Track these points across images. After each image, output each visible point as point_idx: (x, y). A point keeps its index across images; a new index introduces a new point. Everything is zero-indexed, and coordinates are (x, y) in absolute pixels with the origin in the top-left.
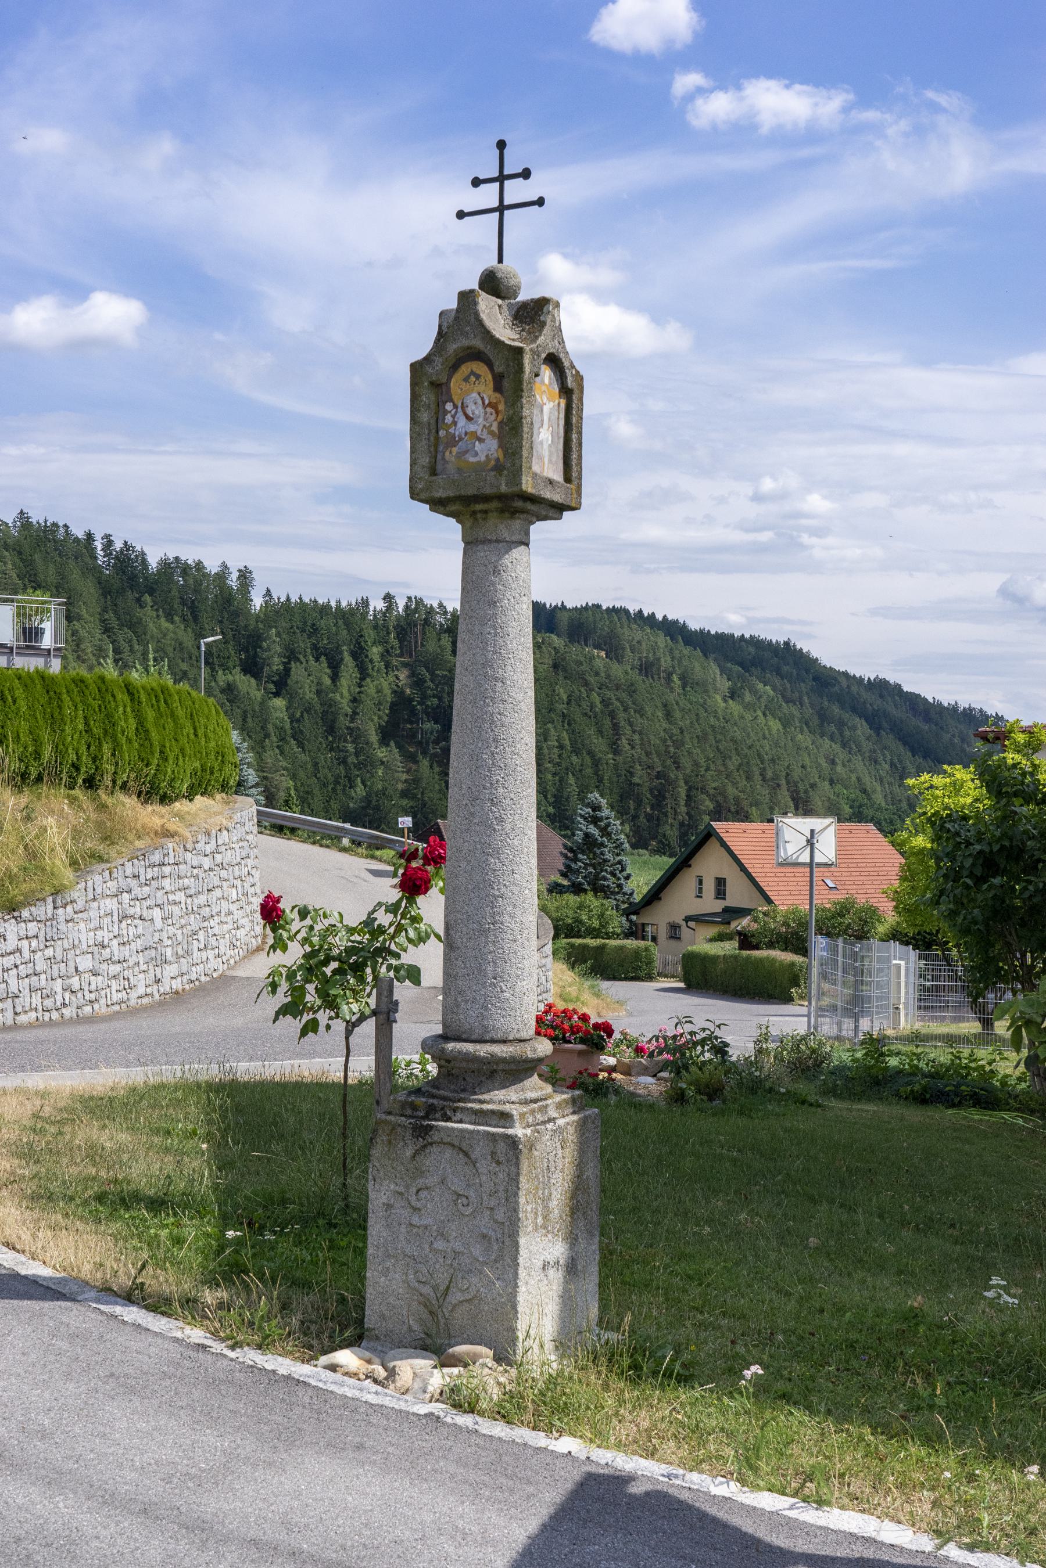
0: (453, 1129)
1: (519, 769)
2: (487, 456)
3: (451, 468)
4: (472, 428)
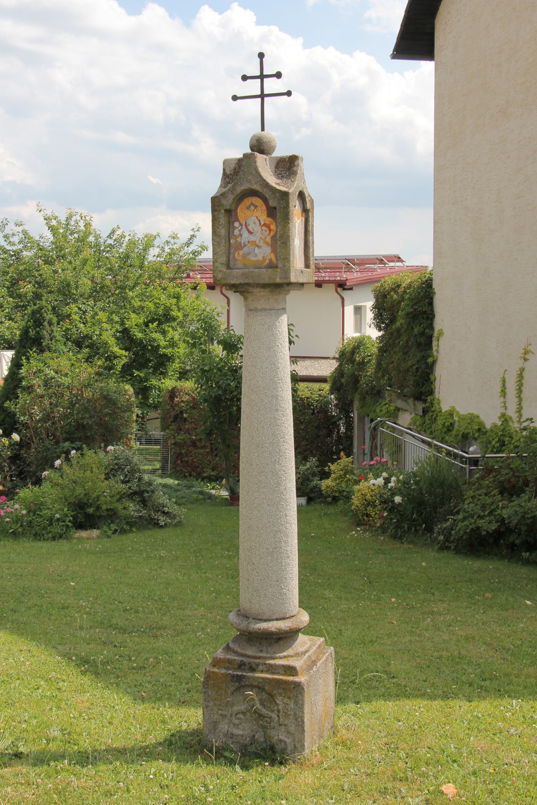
0: (258, 678)
1: (287, 451)
2: (263, 257)
3: (239, 264)
4: (252, 238)
